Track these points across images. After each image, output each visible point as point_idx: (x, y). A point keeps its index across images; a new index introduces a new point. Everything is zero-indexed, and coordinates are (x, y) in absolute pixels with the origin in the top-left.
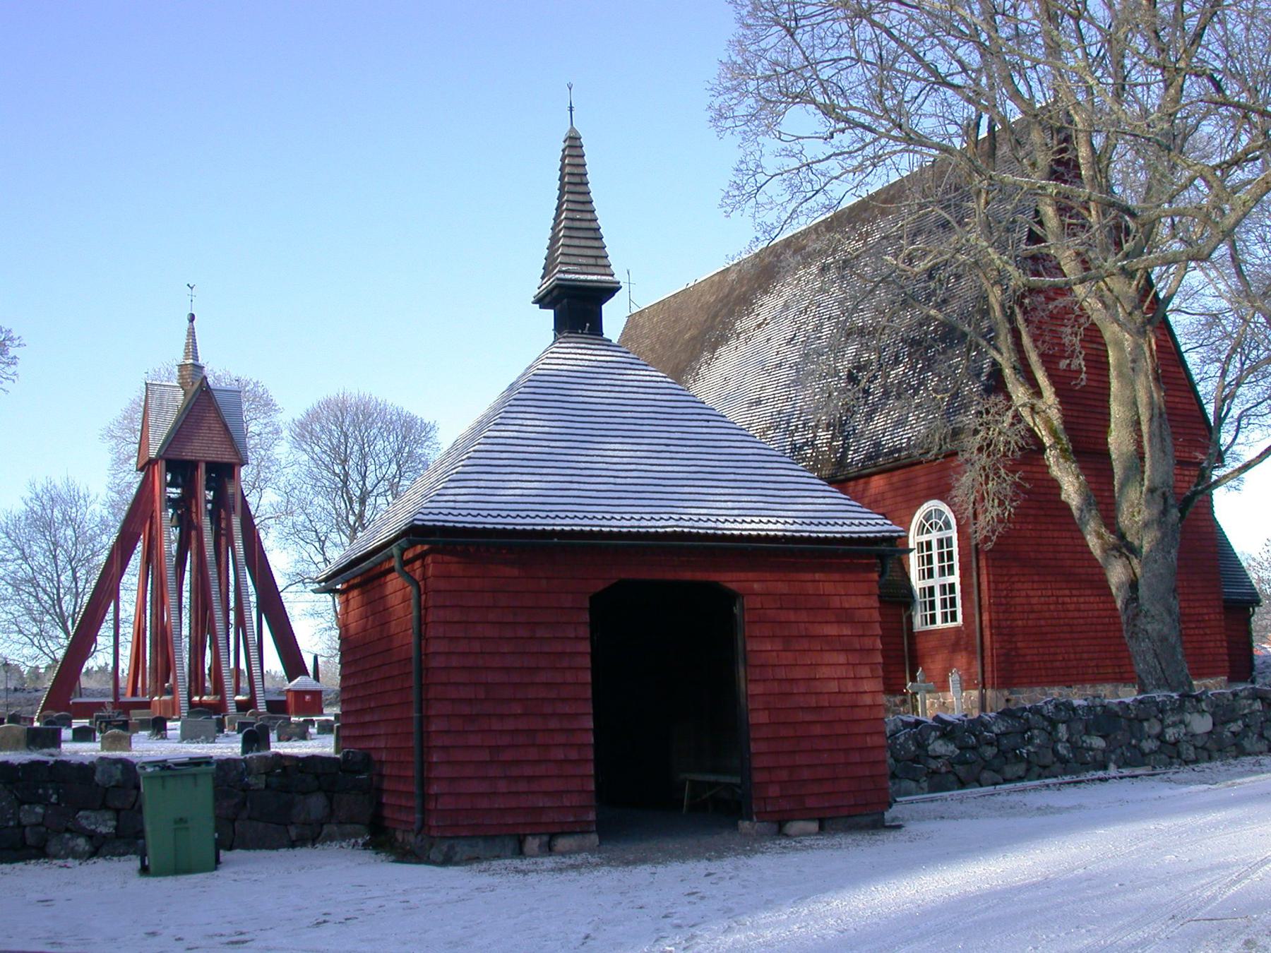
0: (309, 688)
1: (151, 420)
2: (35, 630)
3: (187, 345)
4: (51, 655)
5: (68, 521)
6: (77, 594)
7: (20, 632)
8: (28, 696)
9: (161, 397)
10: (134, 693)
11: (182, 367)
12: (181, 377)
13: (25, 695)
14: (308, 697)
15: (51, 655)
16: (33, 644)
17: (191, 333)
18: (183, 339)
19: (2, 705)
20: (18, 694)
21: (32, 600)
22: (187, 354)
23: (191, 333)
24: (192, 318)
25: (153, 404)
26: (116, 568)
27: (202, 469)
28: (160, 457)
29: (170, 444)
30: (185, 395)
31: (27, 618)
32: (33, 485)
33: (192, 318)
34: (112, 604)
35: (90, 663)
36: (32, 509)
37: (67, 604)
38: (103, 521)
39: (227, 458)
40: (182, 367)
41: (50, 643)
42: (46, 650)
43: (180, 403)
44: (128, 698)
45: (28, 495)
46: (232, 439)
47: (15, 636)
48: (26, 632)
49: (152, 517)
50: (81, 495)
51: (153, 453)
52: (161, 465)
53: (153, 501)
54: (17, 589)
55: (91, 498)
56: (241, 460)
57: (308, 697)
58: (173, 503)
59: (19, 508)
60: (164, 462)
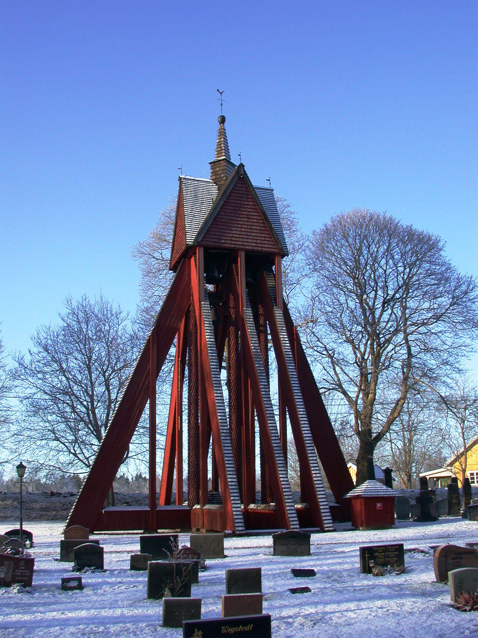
0: (381, 494)
1: (187, 209)
2: (72, 438)
3: (219, 144)
4: (85, 461)
5: (100, 335)
6: (110, 402)
7: (57, 439)
8: (64, 500)
9: (196, 191)
10: (168, 501)
11: (213, 164)
12: (214, 173)
13: (61, 499)
14: (379, 505)
15: (85, 461)
16: (70, 452)
17: (222, 133)
18: (215, 139)
19: (83, 637)
20: (54, 499)
21: (68, 409)
22: (219, 153)
23: (222, 133)
24: (223, 120)
25: (188, 196)
26: (151, 365)
27: (242, 255)
28: (198, 243)
29: (208, 231)
30: (218, 189)
31: (63, 426)
32: (69, 302)
33: (223, 120)
34: (148, 405)
35: (122, 470)
36: (68, 325)
37: (100, 413)
38: (133, 338)
39: (267, 247)
40: (213, 164)
41: (85, 451)
42: (81, 456)
43: (215, 196)
44: (161, 506)
45: (65, 311)
46: (271, 229)
47: (54, 444)
48: (63, 440)
49: (188, 311)
50: (114, 312)
51: (190, 239)
52: (200, 253)
53: (190, 295)
54: (55, 400)
55: (123, 315)
56: (281, 249)
57: (379, 505)
58: (210, 296)
59: (57, 324)
60: (202, 250)
